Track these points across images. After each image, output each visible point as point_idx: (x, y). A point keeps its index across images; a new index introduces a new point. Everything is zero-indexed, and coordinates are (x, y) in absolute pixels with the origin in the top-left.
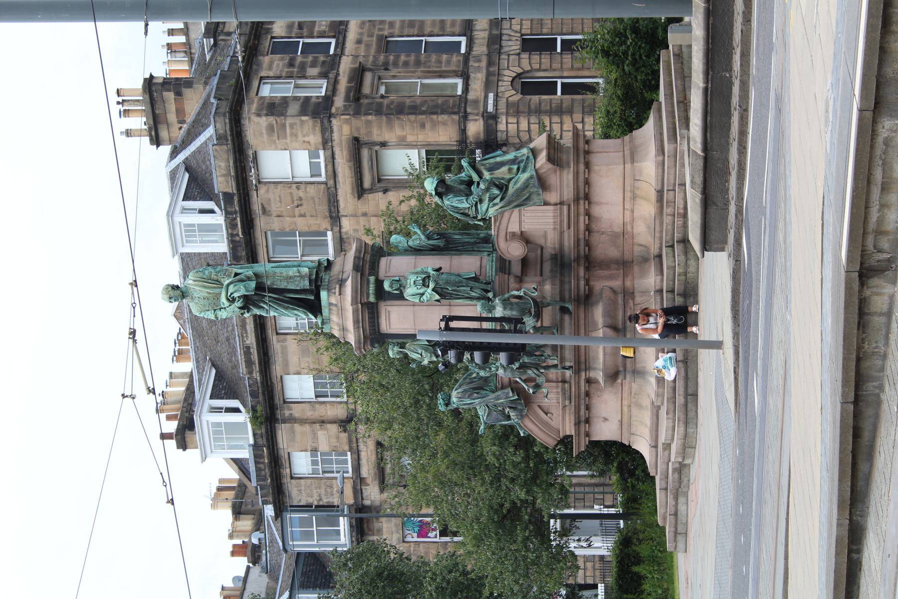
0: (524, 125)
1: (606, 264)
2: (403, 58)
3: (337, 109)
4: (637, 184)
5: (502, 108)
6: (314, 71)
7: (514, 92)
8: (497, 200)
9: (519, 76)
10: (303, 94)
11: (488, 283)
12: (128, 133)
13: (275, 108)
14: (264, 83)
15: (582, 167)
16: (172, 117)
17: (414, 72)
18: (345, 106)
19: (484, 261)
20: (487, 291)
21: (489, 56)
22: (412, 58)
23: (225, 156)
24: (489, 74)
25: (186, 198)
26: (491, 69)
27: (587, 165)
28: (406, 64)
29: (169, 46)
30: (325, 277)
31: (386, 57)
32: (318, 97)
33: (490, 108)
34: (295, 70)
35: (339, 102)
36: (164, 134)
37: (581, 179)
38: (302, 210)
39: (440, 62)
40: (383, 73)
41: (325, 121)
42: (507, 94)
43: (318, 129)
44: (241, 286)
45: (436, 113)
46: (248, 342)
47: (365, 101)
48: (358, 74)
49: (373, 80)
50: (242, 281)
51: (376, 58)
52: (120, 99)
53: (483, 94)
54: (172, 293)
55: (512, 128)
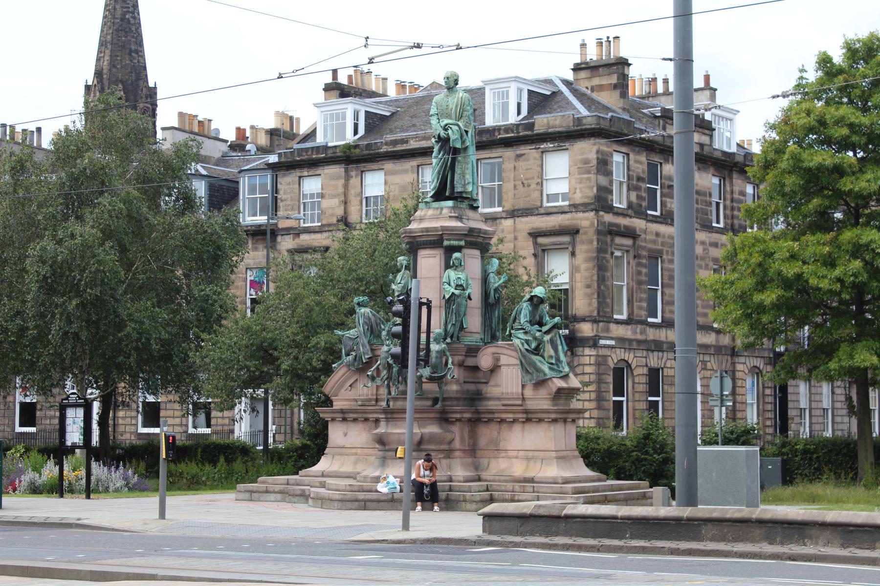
1: (473, 435)
2: (644, 270)
3: (602, 216)
4: (539, 462)
6: (633, 198)
7: (615, 361)
8: (526, 346)
9: (629, 366)
10: (615, 188)
11: (458, 338)
12: (583, 46)
13: (603, 165)
15: (553, 416)
16: (596, 81)
20: (452, 337)
21: (645, 341)
22: (644, 278)
24: (630, 341)
26: (634, 343)
27: (555, 421)
28: (639, 273)
29: (655, 80)
30: (465, 205)
31: (645, 257)
32: (612, 200)
33: (602, 342)
34: (635, 182)
35: (608, 218)
36: (583, 74)
38: (520, 187)
39: (640, 301)
40: (632, 254)
41: (593, 207)
43: (586, 200)
44: (457, 136)
47: (609, 238)
48: (630, 233)
50: (462, 136)
51: (644, 248)
52: (611, 39)
53: (614, 336)
55: (586, 360)
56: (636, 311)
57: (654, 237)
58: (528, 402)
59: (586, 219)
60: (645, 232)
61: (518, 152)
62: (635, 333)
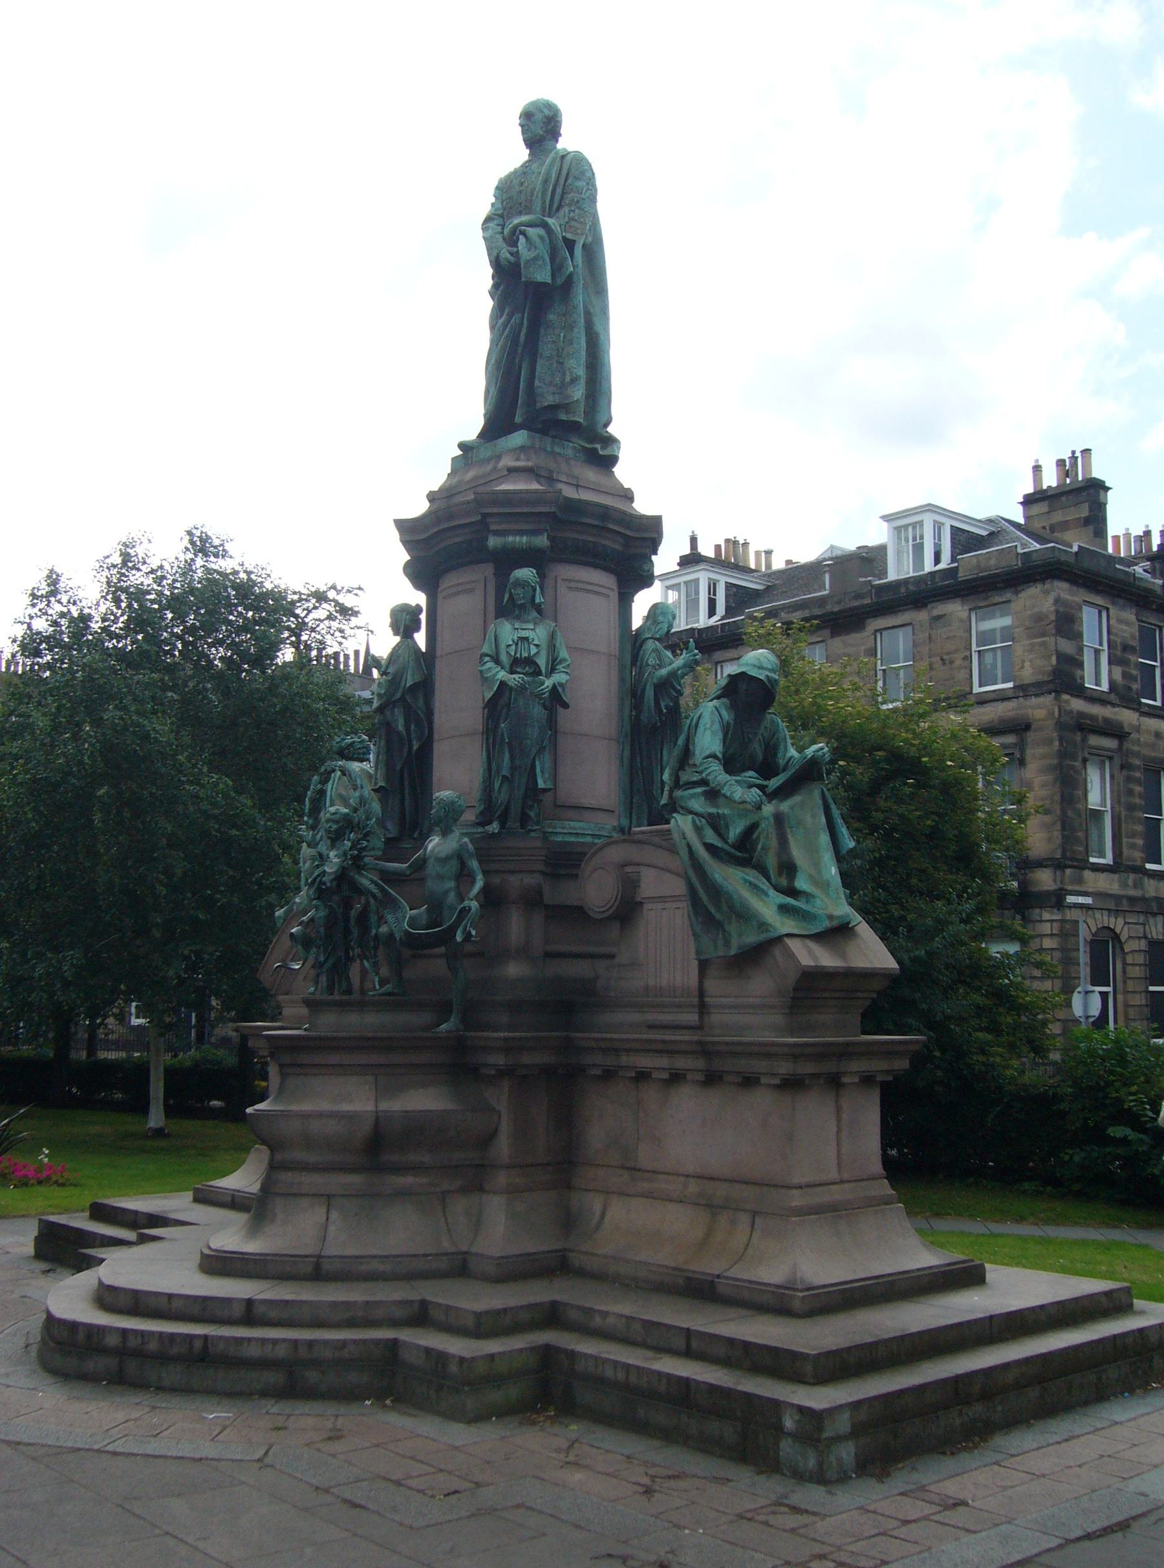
0: (1048, 943)
1: (566, 1119)
2: (1138, 789)
3: (1067, 702)
4: (744, 1219)
5: (1070, 915)
6: (1118, 672)
7: (1094, 930)
8: (711, 837)
9: (1116, 937)
11: (524, 819)
12: (1037, 469)
13: (1066, 623)
14: (1100, 612)
16: (1058, 517)
17: (1119, 802)
18: (1071, 712)
19: (600, 817)
20: (503, 819)
21: (1143, 899)
22: (1137, 801)
23: (1003, 564)
24: (1117, 898)
25: (955, 531)
26: (1125, 902)
27: (792, 1085)
28: (1130, 792)
31: (1138, 768)
32: (1082, 678)
33: (1071, 899)
34: (1119, 653)
35: (1077, 705)
36: (1037, 509)
37: (758, 1066)
38: (938, 665)
39: (1133, 835)
40: (1117, 762)
41: (1051, 686)
42: (1090, 921)
43: (1040, 678)
44: (543, 251)
45: (1063, 828)
46: (783, 615)
47: (1078, 737)
48: (1116, 731)
49: (1109, 750)
50: (553, 253)
51: (1137, 755)
52: (1078, 454)
53: (1090, 890)
54: (539, 117)
55: (1046, 928)
56: (1126, 852)
57: (1152, 739)
58: (715, 1018)
59: (1039, 707)
60: (1138, 729)
61: (936, 612)
62: (1124, 885)
